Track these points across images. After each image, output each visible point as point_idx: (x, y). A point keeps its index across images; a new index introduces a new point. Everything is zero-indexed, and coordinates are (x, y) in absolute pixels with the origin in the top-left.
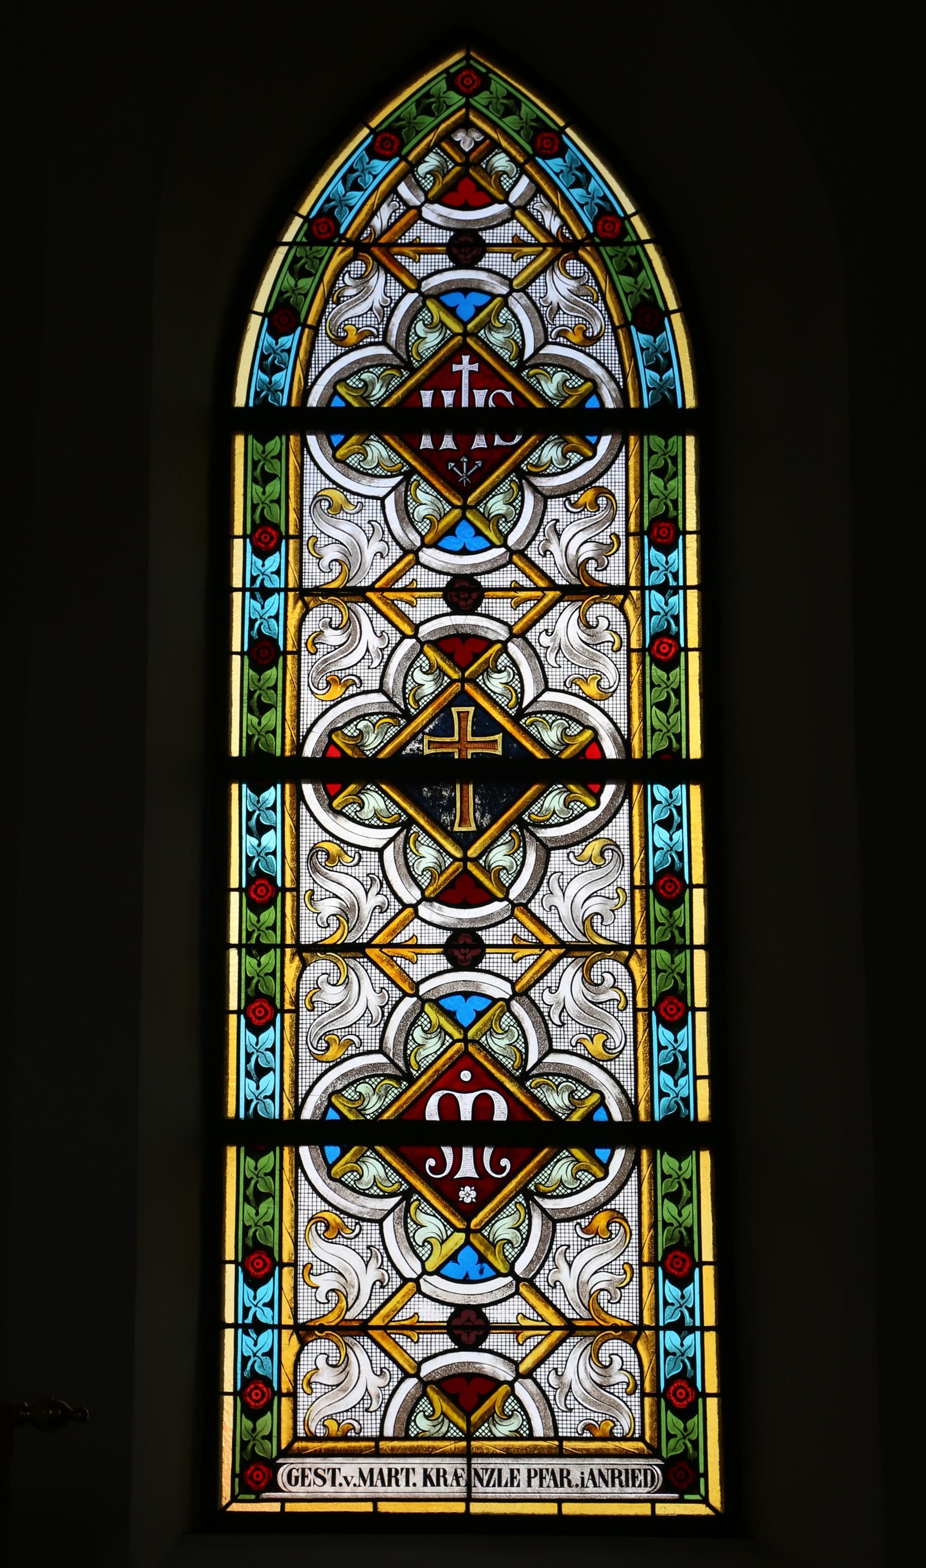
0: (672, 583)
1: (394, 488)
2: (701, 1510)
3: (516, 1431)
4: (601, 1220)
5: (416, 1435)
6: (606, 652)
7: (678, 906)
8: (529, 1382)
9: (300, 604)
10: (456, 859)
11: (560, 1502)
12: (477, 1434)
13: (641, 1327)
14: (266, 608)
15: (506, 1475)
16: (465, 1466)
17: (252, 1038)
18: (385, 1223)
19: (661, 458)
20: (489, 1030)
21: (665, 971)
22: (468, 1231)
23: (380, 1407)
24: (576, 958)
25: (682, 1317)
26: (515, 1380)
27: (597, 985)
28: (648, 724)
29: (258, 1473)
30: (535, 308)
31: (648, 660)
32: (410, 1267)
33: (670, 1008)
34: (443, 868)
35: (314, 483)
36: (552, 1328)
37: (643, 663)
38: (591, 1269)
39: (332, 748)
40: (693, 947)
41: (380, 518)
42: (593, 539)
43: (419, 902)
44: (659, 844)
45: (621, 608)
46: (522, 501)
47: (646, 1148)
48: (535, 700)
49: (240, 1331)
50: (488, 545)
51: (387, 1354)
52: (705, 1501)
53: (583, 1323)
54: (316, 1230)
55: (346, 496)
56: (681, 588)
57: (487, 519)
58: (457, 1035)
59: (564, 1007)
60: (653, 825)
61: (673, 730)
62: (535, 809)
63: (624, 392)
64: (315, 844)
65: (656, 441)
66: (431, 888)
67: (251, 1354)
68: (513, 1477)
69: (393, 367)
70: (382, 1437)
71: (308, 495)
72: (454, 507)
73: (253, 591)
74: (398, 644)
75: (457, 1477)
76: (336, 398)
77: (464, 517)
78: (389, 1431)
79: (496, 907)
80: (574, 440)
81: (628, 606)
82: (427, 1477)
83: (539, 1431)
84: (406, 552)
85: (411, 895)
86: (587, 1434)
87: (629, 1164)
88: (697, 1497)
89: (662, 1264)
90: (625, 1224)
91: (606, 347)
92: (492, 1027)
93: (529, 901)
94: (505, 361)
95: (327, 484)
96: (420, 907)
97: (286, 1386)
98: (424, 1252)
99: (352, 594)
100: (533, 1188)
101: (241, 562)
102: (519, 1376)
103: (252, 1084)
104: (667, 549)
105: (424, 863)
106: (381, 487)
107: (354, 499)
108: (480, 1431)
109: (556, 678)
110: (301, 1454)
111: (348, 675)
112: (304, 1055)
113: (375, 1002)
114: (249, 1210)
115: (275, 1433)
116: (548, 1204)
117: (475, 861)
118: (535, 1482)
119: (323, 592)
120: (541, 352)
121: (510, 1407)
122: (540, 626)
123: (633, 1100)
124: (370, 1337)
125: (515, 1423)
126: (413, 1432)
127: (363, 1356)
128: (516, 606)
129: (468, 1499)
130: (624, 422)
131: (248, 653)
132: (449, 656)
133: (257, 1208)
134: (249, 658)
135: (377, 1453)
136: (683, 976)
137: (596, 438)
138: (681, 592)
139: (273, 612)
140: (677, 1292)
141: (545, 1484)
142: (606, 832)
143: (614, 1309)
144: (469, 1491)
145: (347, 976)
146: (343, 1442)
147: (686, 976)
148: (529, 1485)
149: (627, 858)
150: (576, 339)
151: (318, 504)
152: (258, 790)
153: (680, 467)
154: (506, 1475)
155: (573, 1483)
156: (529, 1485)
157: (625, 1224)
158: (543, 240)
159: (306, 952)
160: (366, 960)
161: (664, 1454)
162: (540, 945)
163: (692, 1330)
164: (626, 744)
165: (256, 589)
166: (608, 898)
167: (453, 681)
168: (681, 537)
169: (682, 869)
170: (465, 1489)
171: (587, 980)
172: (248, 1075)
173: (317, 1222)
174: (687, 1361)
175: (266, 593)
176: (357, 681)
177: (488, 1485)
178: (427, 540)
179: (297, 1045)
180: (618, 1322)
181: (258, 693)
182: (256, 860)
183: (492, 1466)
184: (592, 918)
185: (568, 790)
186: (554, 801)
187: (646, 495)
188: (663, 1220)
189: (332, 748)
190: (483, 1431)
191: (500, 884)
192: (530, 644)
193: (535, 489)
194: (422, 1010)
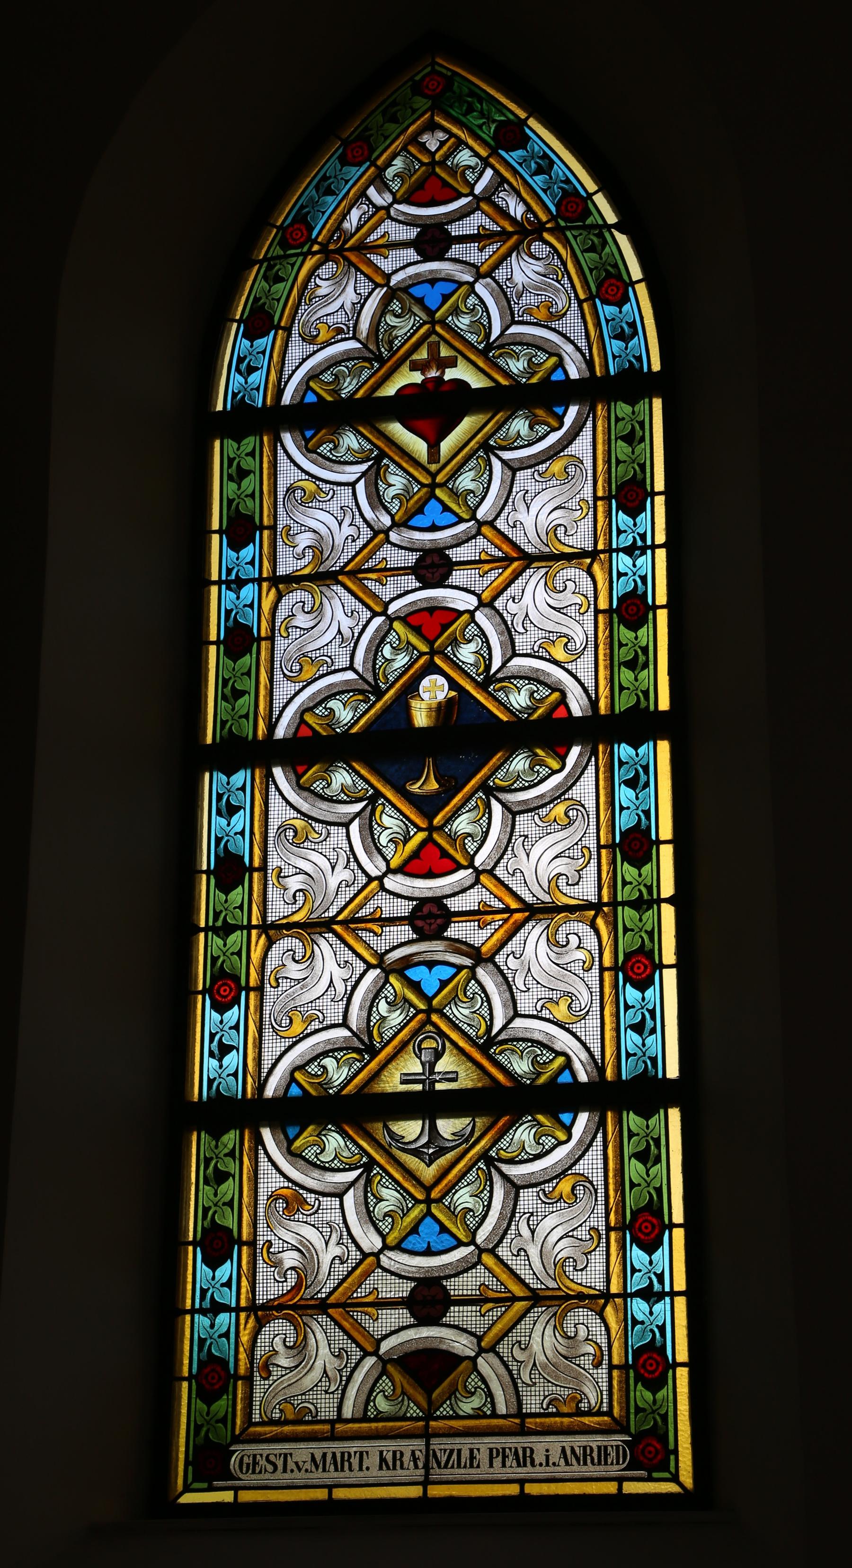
0: (657, 1287)
1: (364, 474)
2: (670, 1488)
3: (479, 1409)
4: (565, 1186)
5: (375, 1416)
6: (577, 972)
7: (660, 1388)
8: (491, 1357)
9: (273, 590)
10: (423, 485)
11: (522, 1482)
12: (438, 1413)
13: (607, 1296)
14: (232, 824)
15: (465, 1454)
16: (423, 1448)
17: (216, 1016)
18: (357, 486)
19: (637, 936)
20: (454, 999)
21: (632, 930)
22: (428, 1201)
23: (341, 1235)
24: (548, 1307)
25: (651, 1283)
26: (478, 1355)
27: (563, 946)
28: (616, 638)
29: (211, 1464)
30: (502, 293)
31: (616, 620)
32: (371, 1241)
33: (638, 967)
34: (411, 494)
35: (287, 475)
36: (514, 1299)
37: (614, 862)
38: (555, 1237)
39: (303, 726)
40: (660, 901)
41: (345, 845)
42: (570, 1234)
43: (385, 875)
44: (621, 457)
45: (590, 572)
46: (491, 1192)
47: (611, 1110)
48: (504, 1027)
49: (224, 587)
50: (455, 520)
51: (351, 948)
52: (675, 1478)
53: (550, 1293)
54: (286, 836)
55: (318, 486)
56: (667, 1294)
57: (456, 494)
58: (422, 1006)
59: (527, 615)
60: (620, 785)
61: (639, 573)
62: (500, 774)
63: (590, 363)
64: (272, 1192)
65: (623, 409)
66: (400, 514)
67: (208, 1336)
68: (472, 1457)
69: (365, 359)
70: (340, 1419)
71: (274, 824)
72: (417, 1201)
73: (228, 583)
74: (362, 976)
75: (415, 1460)
76: (310, 393)
77: (429, 1213)
78: (347, 1413)
79: (463, 201)
80: (540, 412)
81: (600, 922)
82: (383, 1460)
83: (502, 1409)
84: (376, 533)
85: (371, 1241)
86: (552, 1410)
87: (593, 1127)
88: (666, 1475)
89: (630, 1227)
90: (581, 465)
91: (572, 323)
92: (457, 995)
93: (497, 1246)
94: (473, 344)
95: (294, 814)
96: (386, 880)
97: (242, 1371)
98: (385, 1227)
99: (323, 578)
100: (494, 1154)
101: (218, 555)
102: (481, 1351)
103: (214, 1063)
104: (642, 985)
105: (392, 492)
106: (352, 472)
107: (326, 487)
108: (441, 1409)
109: (525, 1004)
110: (257, 1439)
111: (321, 650)
112: (278, 676)
113: (339, 974)
114: (233, 486)
115: (230, 1416)
116: (507, 455)
117: (440, 828)
118: (498, 1462)
119: (293, 580)
120: (507, 333)
121: (473, 1383)
122: (508, 949)
123: (593, 696)
124: (329, 1316)
125: (476, 1402)
126: (371, 1413)
127: (326, 947)
128: (481, 250)
129: (426, 1483)
130: (594, 391)
131: (224, 642)
132: (417, 630)
133: (220, 1060)
134: (215, 878)
135: (333, 1437)
136: (651, 934)
137: (571, 1116)
138: (649, 552)
139: (239, 828)
140: (638, 994)
141: (508, 1464)
142: (569, 449)
143: (579, 1277)
144: (427, 1474)
145: (321, 603)
146: (299, 1425)
147: (654, 934)
148: (491, 1466)
149: (590, 472)
150: (542, 315)
151: (283, 834)
152: (217, 1135)
153: (663, 1151)
154: (465, 1454)
155: (537, 1462)
156: (491, 1466)
157: (581, 465)
158: (510, 229)
159: (273, 931)
160: (331, 935)
161: (633, 1430)
162: (507, 910)
163: (661, 1296)
164: (594, 703)
165: (232, 581)
166: (581, 1240)
167: (422, 654)
168: (655, 847)
169: (646, 592)
170: (422, 1472)
171: (552, 942)
172: (212, 1054)
173: (285, 830)
174: (640, 694)
175: (240, 583)
176: (320, 1015)
177: (446, 1467)
178: (398, 195)
179: (272, 668)
180: (586, 1291)
181: (226, 839)
182: (205, 1429)
183: (450, 1447)
184: (556, 530)
185: (534, 415)
186: (519, 763)
187: (613, 461)
188: (629, 1130)
189: (303, 726)
190: (445, 1410)
191: (467, 182)
192: (497, 611)
193: (505, 1177)
194: (387, 981)
